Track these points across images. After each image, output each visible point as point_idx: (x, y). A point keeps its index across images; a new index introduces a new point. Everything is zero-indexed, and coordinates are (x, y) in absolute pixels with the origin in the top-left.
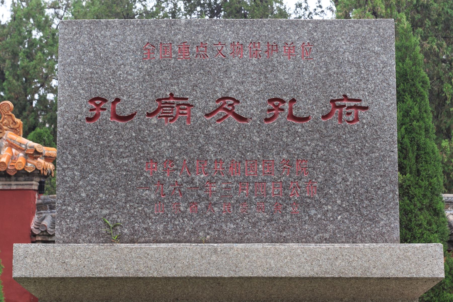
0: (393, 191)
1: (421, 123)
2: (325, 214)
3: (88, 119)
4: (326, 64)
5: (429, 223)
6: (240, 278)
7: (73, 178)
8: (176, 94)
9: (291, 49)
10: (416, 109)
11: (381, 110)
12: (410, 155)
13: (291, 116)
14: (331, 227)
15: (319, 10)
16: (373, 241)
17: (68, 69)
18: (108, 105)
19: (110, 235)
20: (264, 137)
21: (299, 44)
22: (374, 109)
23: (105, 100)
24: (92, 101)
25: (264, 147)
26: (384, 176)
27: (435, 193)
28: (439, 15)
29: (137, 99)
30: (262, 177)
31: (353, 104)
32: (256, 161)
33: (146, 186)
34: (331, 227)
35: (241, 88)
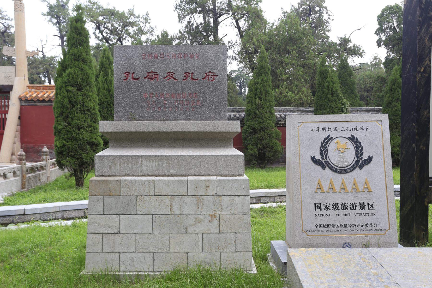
0: (226, 104)
1: (267, 83)
2: (203, 111)
3: (124, 79)
4: (204, 60)
5: (269, 117)
6: (174, 132)
7: (119, 99)
8: (154, 71)
9: (192, 55)
10: (266, 78)
11: (222, 76)
12: (263, 94)
13: (192, 78)
14: (205, 115)
15: (236, 44)
16: (219, 120)
17: (117, 62)
18: (131, 75)
19: (132, 118)
20: (183, 85)
21: (195, 54)
22: (220, 76)
23: (130, 73)
24: (125, 73)
25: (183, 89)
26: (223, 98)
27: (271, 107)
28: (276, 45)
29: (140, 72)
30: (182, 99)
31: (213, 74)
32: (180, 94)
33: (144, 102)
34: (205, 115)
35: (175, 69)
